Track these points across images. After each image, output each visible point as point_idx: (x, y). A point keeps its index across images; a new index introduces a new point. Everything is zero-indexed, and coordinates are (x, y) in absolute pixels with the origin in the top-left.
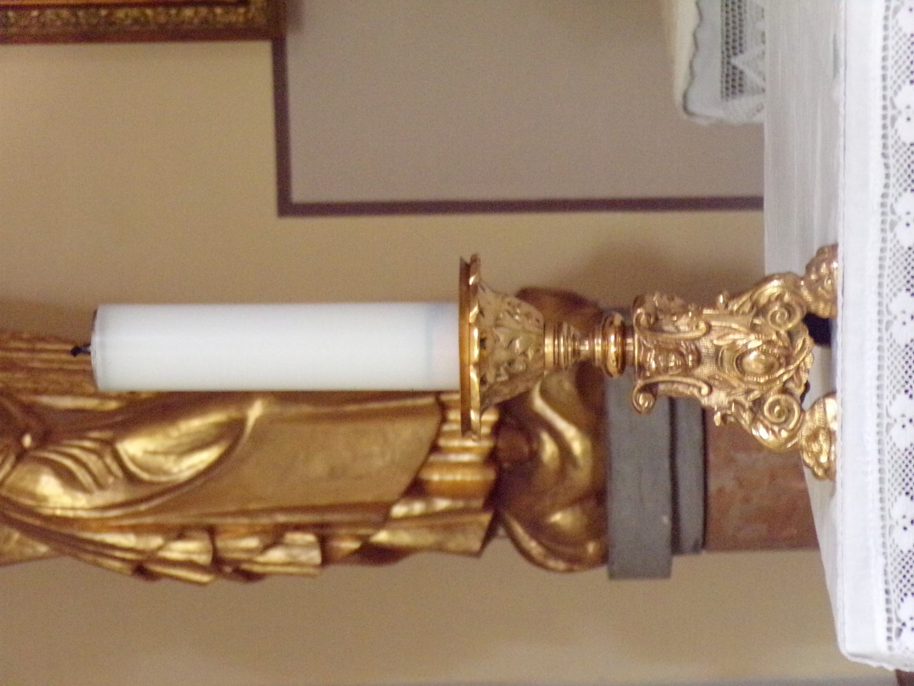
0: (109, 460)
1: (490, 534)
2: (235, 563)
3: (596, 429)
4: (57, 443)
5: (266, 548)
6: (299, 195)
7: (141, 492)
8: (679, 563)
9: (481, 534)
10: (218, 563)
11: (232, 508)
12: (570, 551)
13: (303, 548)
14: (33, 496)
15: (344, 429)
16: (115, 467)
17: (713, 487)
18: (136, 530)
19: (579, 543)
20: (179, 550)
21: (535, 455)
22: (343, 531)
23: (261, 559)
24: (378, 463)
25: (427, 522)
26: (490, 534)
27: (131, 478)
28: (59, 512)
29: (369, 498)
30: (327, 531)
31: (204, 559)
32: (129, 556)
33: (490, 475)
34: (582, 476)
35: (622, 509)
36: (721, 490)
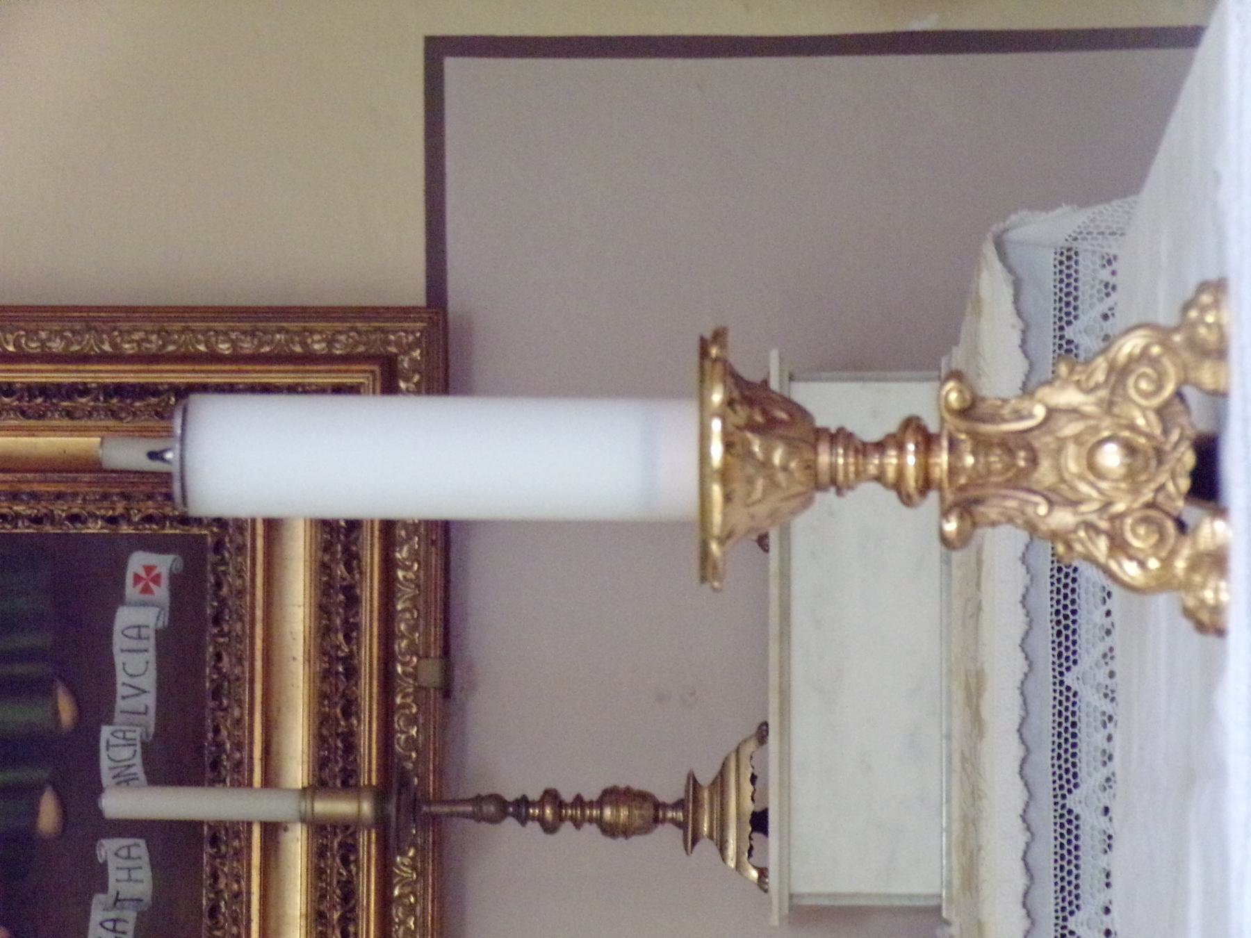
6: (452, 65)
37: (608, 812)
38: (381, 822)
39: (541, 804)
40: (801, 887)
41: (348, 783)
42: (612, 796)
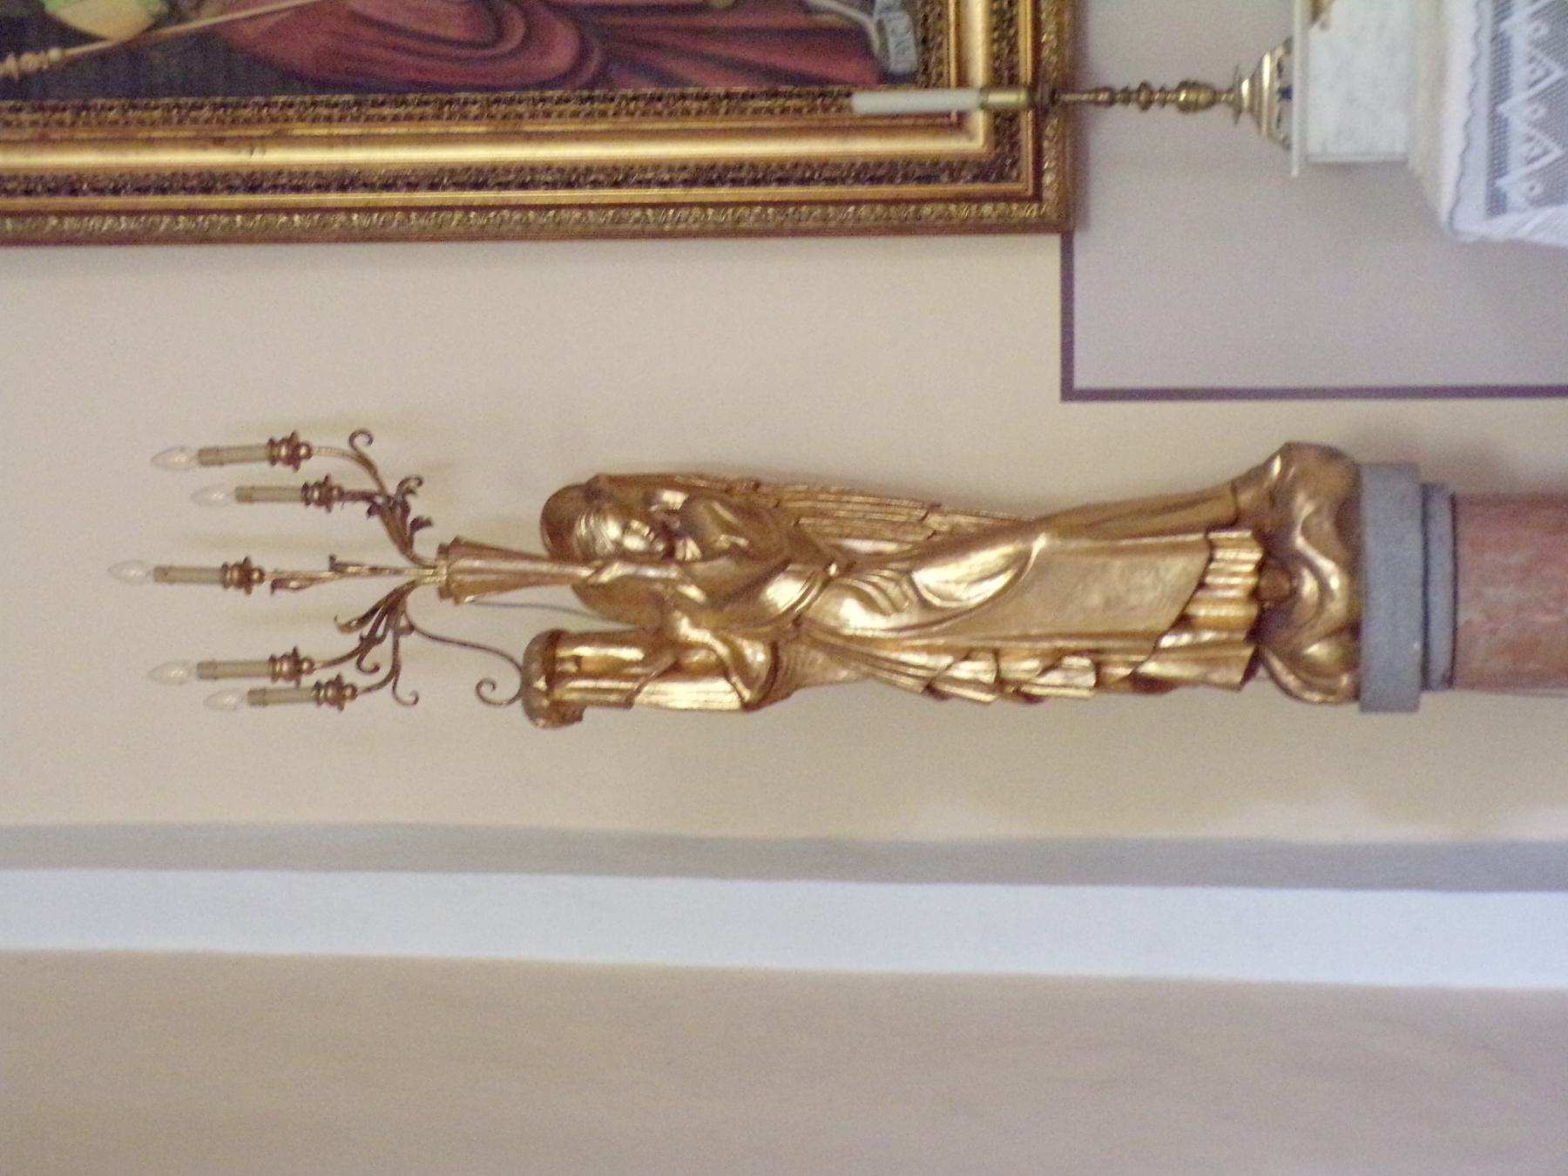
0: (906, 587)
1: (1249, 673)
2: (1019, 683)
3: (1353, 567)
4: (858, 571)
5: (1046, 670)
6: (1081, 381)
7: (933, 617)
8: (1426, 698)
9: (1242, 667)
10: (1000, 684)
11: (1015, 632)
12: (1324, 682)
13: (1078, 675)
14: (837, 618)
15: (1118, 564)
16: (910, 593)
17: (1462, 618)
18: (930, 650)
19: (1334, 676)
20: (965, 670)
21: (1294, 593)
22: (1116, 658)
23: (1042, 680)
24: (1149, 597)
25: (1194, 655)
26: (1249, 673)
27: (925, 604)
28: (859, 633)
29: (1140, 626)
30: (1101, 658)
31: (989, 678)
32: (920, 673)
33: (1253, 611)
34: (1337, 609)
35: (1376, 636)
36: (1469, 623)
37: (1183, 96)
38: (1032, 105)
39: (1139, 91)
40: (1314, 147)
41: (1012, 82)
42: (1184, 85)
